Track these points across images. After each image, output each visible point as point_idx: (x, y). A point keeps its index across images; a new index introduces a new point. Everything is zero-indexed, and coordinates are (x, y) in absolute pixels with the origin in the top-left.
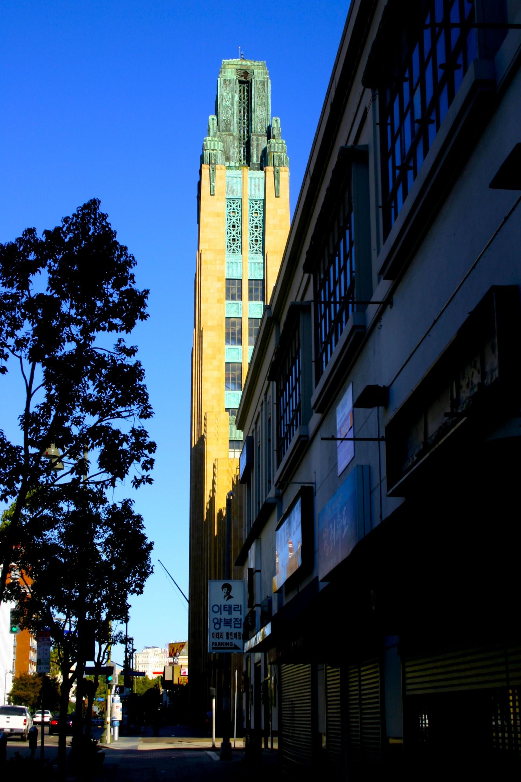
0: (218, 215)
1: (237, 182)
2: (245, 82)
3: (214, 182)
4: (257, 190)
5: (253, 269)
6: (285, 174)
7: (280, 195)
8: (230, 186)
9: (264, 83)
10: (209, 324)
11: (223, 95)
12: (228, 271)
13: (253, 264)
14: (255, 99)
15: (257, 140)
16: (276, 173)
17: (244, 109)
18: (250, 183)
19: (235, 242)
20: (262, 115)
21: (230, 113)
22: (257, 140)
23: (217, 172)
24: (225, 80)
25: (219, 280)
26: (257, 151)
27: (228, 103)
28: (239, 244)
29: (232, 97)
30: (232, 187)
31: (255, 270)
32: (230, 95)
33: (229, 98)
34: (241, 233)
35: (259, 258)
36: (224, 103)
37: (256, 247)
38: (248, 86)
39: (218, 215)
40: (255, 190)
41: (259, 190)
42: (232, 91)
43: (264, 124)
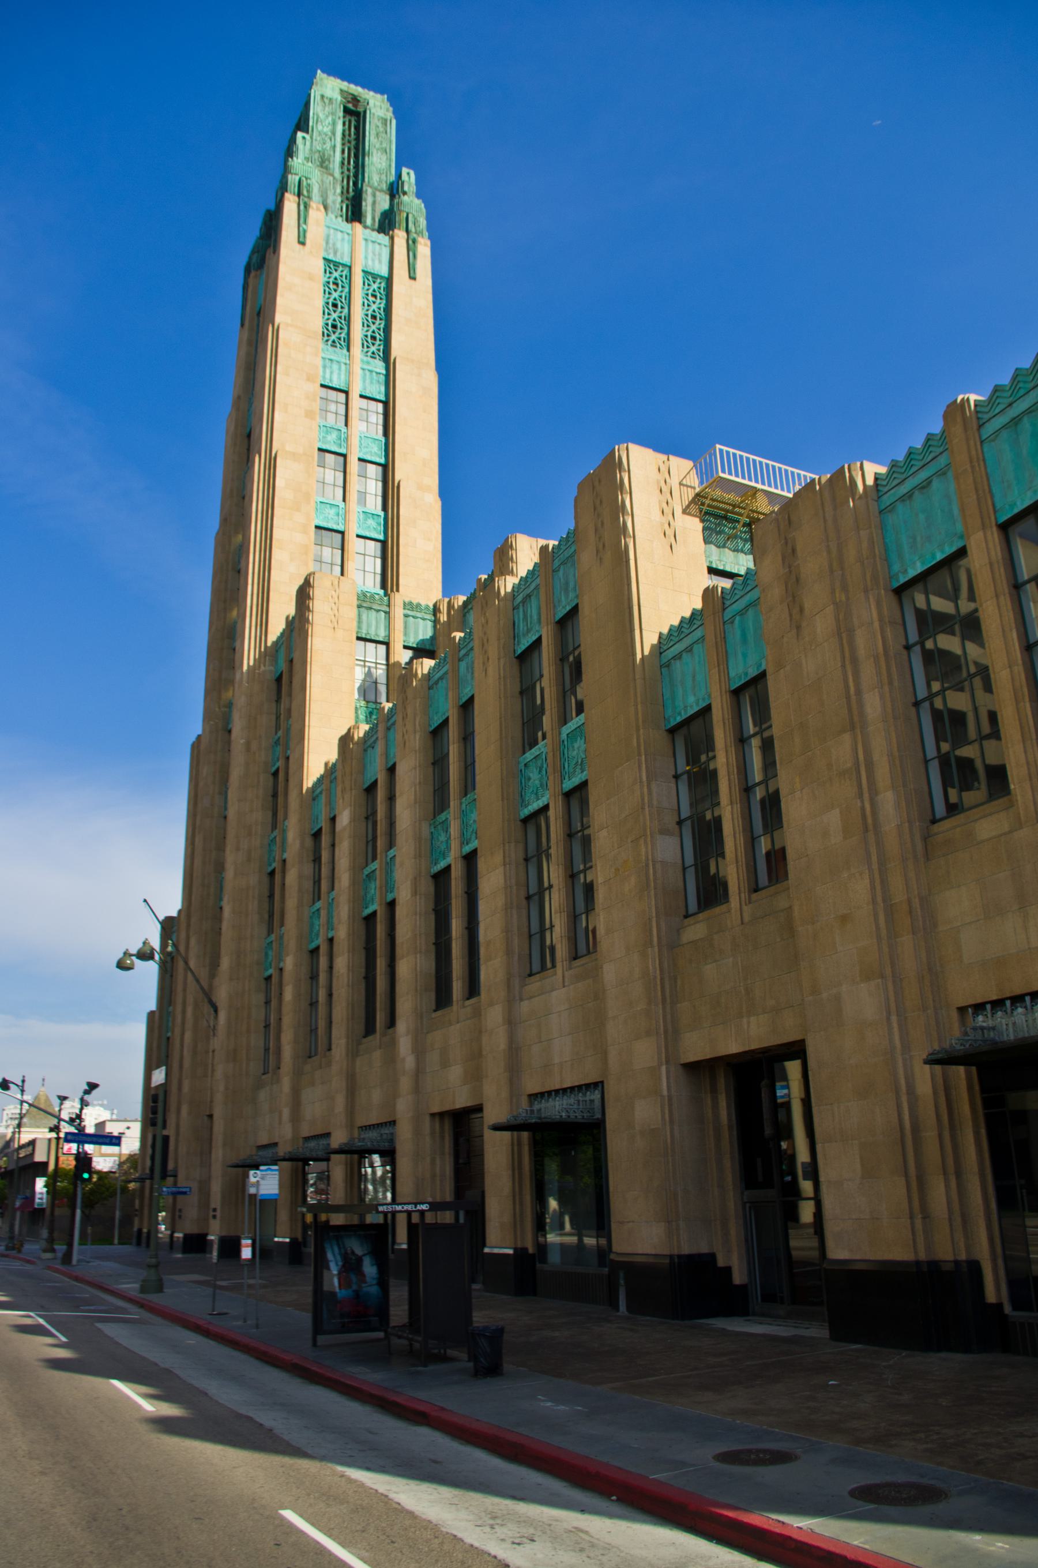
0: (311, 278)
1: (343, 239)
2: (355, 114)
3: (305, 222)
4: (377, 262)
5: (368, 381)
6: (424, 249)
7: (418, 276)
8: (331, 241)
9: (385, 122)
10: (289, 448)
11: (318, 117)
12: (324, 372)
13: (368, 373)
14: (371, 139)
15: (374, 195)
16: (410, 242)
17: (349, 149)
18: (366, 249)
19: (336, 331)
20: (380, 163)
21: (328, 145)
22: (374, 195)
23: (312, 213)
24: (322, 97)
25: (310, 379)
26: (374, 210)
27: (327, 130)
28: (343, 335)
29: (334, 124)
30: (334, 244)
31: (371, 383)
32: (330, 119)
33: (326, 123)
34: (348, 319)
35: (379, 366)
36: (320, 128)
37: (373, 349)
38: (358, 121)
39: (311, 278)
40: (373, 260)
41: (380, 262)
42: (333, 114)
43: (384, 177)
